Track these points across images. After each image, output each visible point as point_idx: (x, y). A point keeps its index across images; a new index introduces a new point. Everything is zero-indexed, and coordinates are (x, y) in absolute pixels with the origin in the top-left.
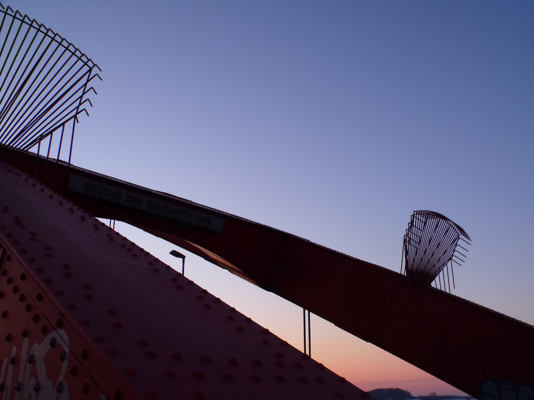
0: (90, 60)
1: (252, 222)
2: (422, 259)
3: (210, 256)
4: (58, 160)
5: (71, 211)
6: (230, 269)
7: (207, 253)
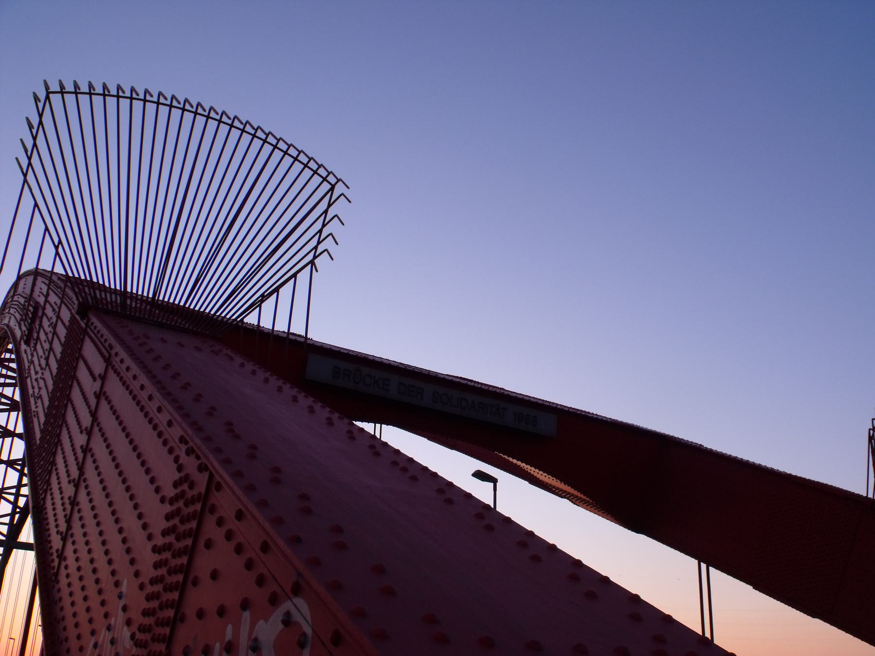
0: (302, 151)
1: (605, 419)
3: (538, 477)
4: (289, 333)
5: (311, 410)
6: (572, 497)
7: (532, 473)
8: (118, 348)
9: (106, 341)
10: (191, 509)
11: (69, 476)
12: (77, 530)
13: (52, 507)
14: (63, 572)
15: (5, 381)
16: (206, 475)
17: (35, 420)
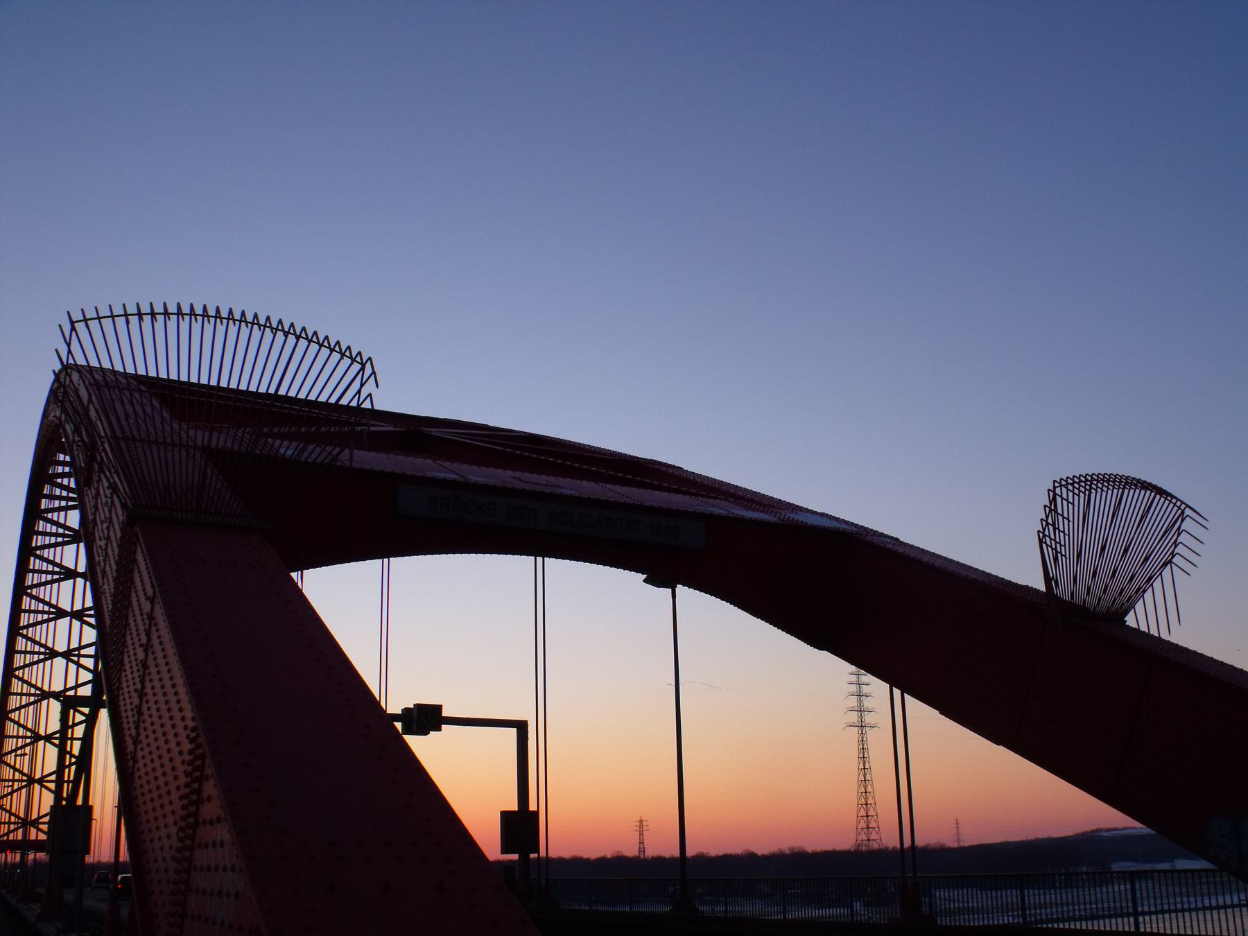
2: (1089, 589)
12: (155, 642)
15: (56, 540)
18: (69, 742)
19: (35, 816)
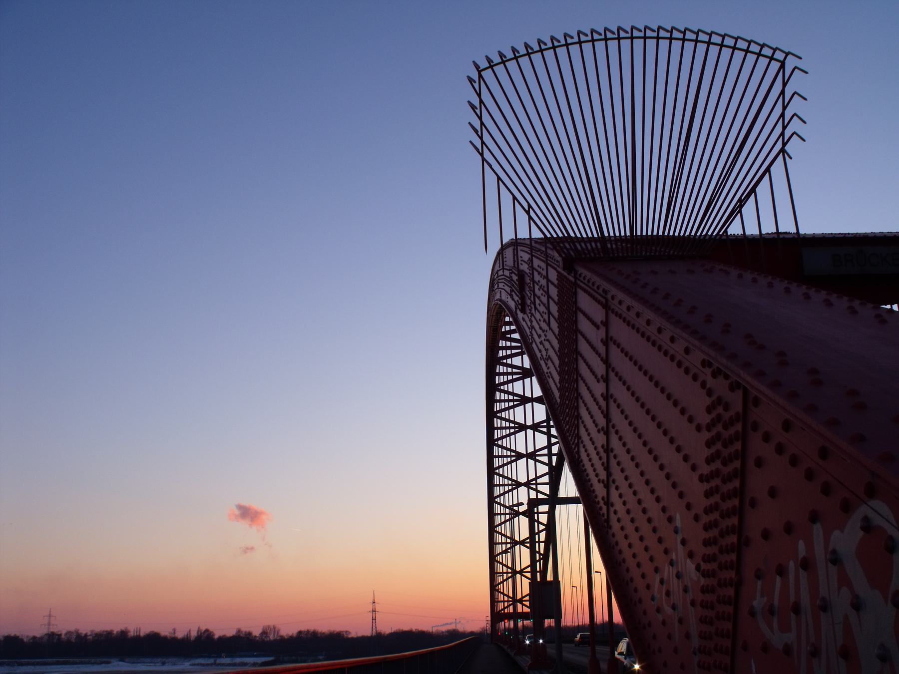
0: (726, 35)
4: (778, 233)
5: (828, 303)
8: (613, 291)
9: (598, 287)
10: (732, 431)
11: (596, 426)
13: (588, 458)
14: (613, 518)
15: (511, 352)
16: (739, 394)
17: (550, 381)
18: (537, 544)
19: (519, 597)
